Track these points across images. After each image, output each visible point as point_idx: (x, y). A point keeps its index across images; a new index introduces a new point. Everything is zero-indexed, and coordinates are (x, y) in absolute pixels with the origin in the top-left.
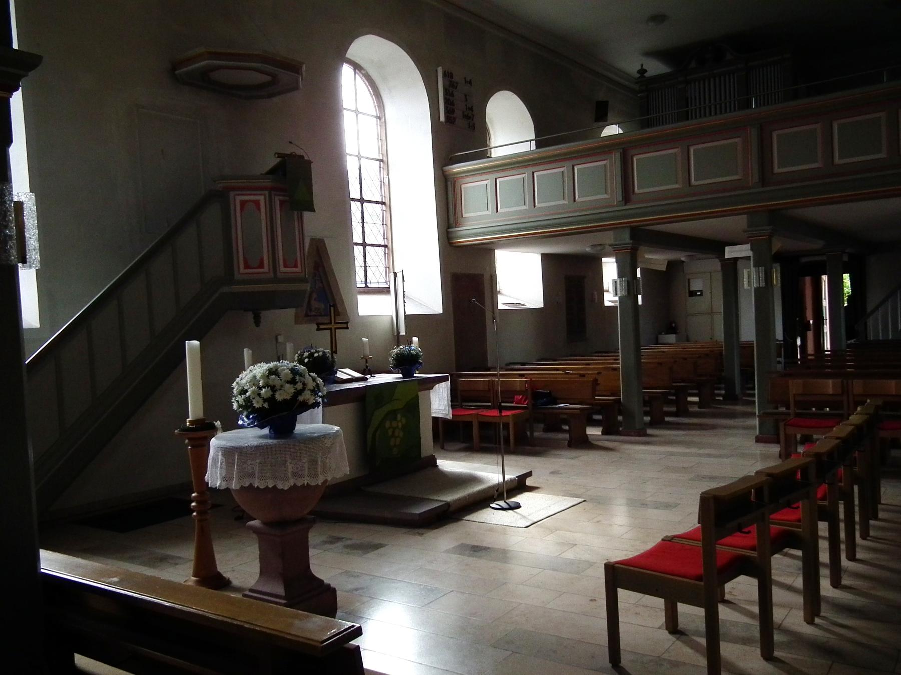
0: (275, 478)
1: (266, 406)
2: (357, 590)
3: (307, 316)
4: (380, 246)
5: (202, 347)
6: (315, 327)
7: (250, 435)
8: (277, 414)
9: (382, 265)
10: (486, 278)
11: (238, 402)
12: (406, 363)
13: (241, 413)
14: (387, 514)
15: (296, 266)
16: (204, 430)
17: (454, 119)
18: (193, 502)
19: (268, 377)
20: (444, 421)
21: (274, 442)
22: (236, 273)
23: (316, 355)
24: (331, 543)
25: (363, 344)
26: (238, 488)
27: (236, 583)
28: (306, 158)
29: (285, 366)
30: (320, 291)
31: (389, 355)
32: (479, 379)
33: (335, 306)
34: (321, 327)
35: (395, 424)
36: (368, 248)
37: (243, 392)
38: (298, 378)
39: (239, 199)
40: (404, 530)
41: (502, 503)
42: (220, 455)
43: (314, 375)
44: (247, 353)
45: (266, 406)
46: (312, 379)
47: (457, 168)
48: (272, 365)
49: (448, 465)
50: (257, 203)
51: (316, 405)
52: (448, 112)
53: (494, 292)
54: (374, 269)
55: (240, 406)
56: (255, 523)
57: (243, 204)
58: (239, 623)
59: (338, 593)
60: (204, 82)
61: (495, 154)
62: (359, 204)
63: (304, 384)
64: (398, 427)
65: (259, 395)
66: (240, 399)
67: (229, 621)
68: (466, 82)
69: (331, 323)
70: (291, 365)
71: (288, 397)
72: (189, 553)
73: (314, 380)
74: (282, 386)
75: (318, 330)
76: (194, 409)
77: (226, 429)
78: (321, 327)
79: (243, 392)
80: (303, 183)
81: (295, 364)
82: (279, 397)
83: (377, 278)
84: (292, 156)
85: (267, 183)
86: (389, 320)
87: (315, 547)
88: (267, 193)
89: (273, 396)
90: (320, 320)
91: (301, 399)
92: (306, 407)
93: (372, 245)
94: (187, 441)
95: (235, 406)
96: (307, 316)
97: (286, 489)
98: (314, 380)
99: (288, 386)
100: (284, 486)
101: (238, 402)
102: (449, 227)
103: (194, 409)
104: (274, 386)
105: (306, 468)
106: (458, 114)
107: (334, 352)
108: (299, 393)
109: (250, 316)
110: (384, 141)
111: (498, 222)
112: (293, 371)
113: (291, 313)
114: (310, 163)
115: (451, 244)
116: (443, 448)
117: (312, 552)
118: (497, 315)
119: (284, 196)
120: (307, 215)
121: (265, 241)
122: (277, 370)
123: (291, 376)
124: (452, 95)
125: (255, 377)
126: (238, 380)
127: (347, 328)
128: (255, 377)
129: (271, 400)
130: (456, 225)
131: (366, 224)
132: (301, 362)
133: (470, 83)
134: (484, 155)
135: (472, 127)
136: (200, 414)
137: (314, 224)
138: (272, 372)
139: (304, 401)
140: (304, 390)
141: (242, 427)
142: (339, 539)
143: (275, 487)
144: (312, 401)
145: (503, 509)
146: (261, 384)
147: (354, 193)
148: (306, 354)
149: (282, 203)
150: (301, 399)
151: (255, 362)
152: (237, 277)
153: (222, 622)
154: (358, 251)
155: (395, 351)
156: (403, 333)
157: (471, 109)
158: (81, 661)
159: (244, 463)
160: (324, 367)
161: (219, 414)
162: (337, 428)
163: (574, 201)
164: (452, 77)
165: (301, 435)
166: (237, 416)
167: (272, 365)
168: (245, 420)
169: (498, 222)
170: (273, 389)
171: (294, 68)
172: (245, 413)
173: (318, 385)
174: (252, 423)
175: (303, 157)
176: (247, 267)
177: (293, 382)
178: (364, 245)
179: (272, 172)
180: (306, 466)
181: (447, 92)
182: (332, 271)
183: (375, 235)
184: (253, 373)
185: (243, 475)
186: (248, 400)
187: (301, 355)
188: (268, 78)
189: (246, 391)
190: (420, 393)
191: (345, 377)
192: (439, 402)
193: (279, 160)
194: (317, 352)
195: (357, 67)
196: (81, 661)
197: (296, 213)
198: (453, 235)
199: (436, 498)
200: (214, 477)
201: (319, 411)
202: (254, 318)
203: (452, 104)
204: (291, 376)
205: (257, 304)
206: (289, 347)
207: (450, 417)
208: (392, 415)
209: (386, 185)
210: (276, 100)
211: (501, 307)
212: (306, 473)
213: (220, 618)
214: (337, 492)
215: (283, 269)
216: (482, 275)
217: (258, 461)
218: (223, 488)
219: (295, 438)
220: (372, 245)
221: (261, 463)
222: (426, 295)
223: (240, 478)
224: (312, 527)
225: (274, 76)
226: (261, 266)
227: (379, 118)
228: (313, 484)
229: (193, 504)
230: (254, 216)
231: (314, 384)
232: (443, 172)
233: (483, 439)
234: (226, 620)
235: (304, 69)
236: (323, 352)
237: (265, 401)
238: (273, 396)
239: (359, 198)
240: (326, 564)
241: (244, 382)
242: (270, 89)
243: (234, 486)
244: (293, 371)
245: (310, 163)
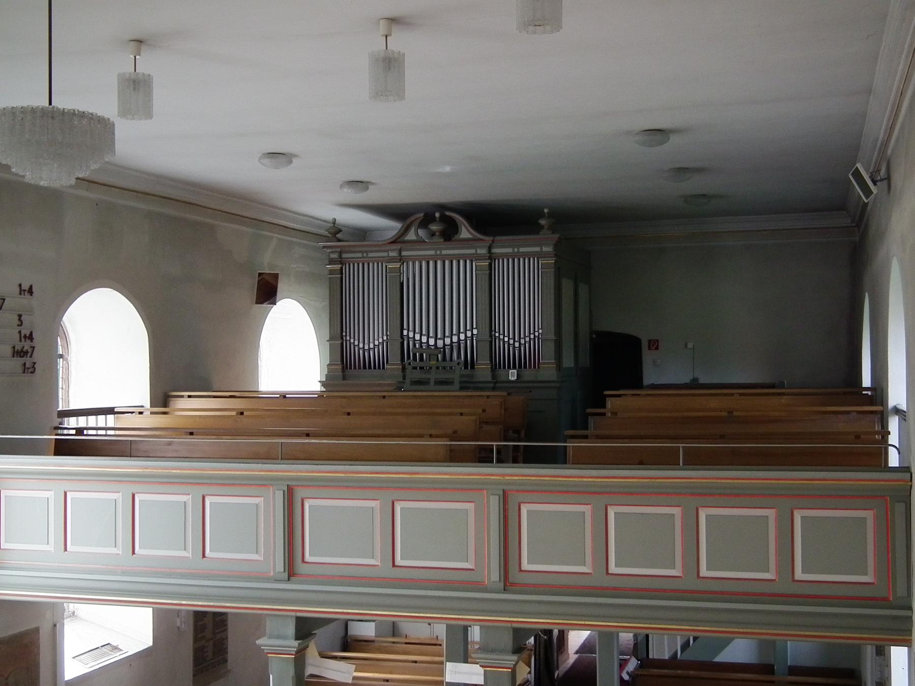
68: (21, 291)
157: (30, 337)
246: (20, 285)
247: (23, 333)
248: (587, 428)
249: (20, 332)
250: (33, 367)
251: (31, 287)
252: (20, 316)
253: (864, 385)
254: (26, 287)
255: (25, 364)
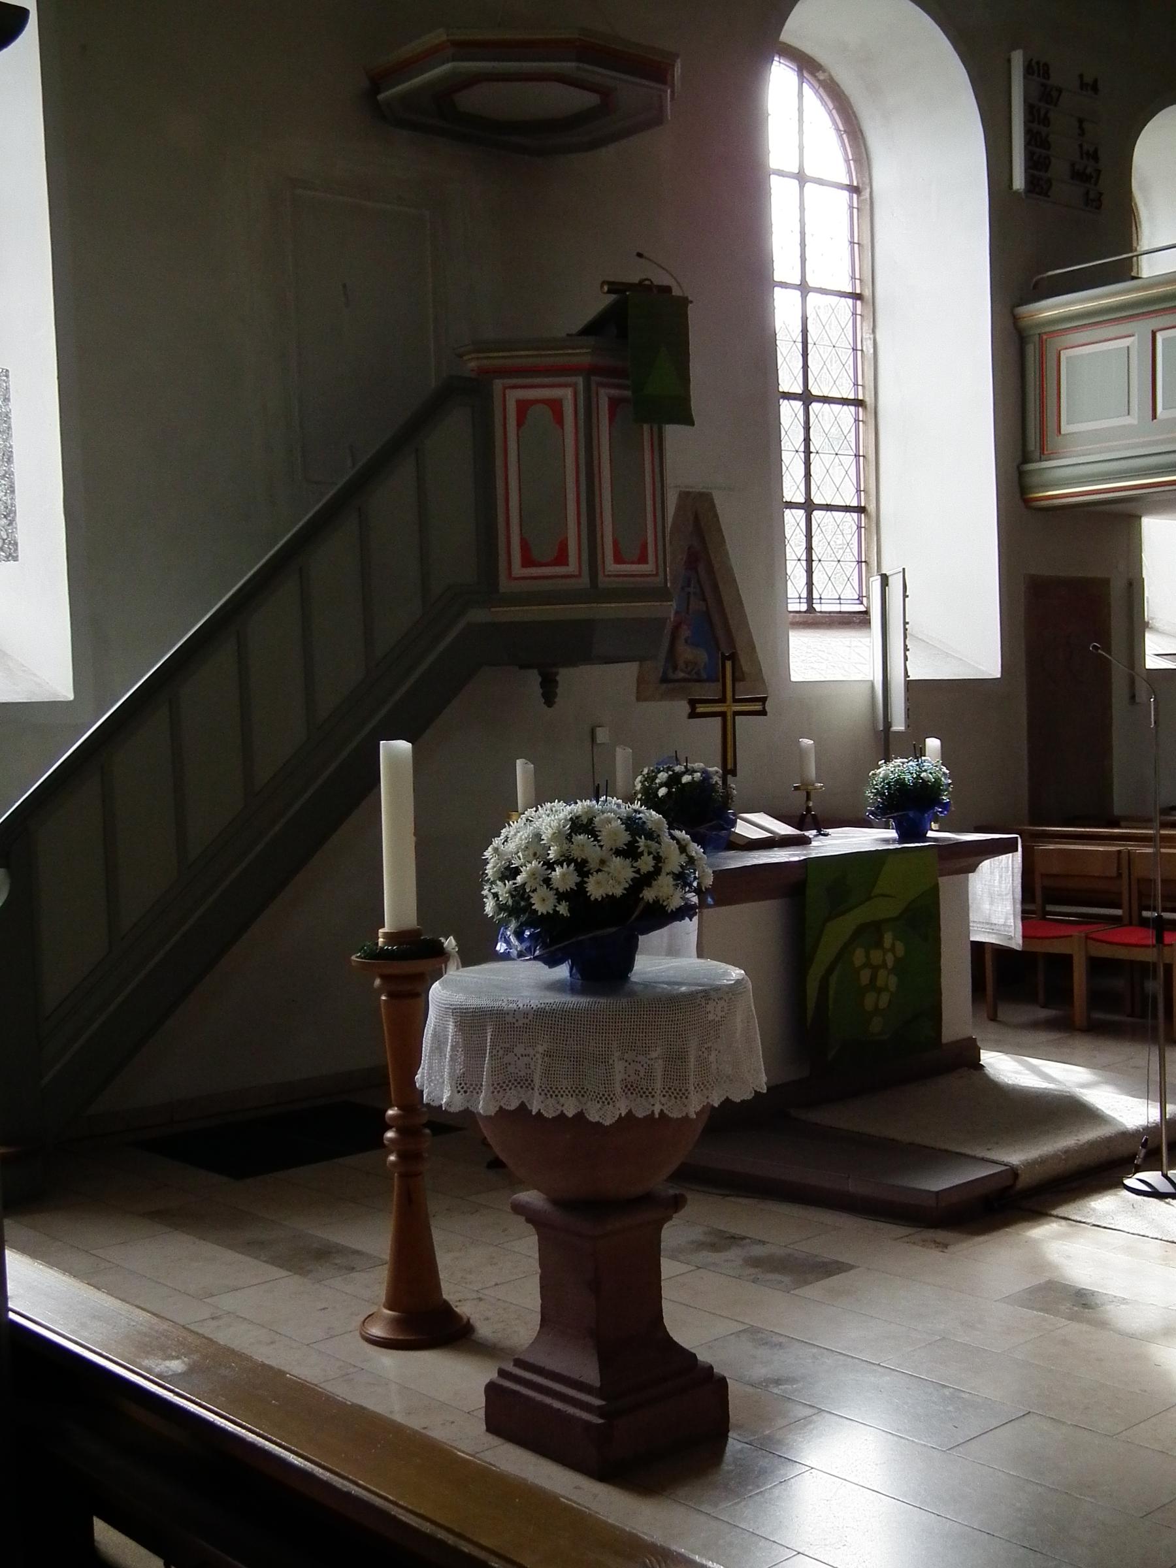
0: (580, 1092)
1: (563, 909)
2: (778, 1382)
3: (665, 680)
4: (847, 509)
5: (418, 755)
6: (683, 707)
7: (521, 980)
8: (592, 932)
9: (851, 556)
10: (1117, 588)
11: (496, 895)
12: (908, 805)
13: (505, 923)
14: (853, 1186)
15: (643, 559)
16: (417, 957)
17: (1049, 182)
18: (388, 1127)
19: (569, 838)
20: (1001, 952)
21: (582, 1001)
22: (503, 578)
23: (686, 779)
24: (713, 1247)
25: (802, 753)
26: (492, 1111)
27: (484, 1330)
28: (676, 292)
29: (612, 809)
30: (706, 633)
31: (866, 780)
32: (1092, 847)
33: (733, 657)
34: (701, 709)
35: (876, 956)
36: (817, 514)
37: (510, 873)
38: (642, 842)
39: (513, 396)
40: (901, 1231)
41: (1153, 1177)
42: (451, 1028)
43: (682, 835)
44: (522, 769)
45: (563, 909)
46: (675, 844)
47: (1051, 309)
48: (579, 807)
49: (1005, 1066)
50: (556, 406)
51: (686, 911)
52: (1034, 163)
53: (1135, 625)
54: (830, 567)
55: (501, 907)
56: (531, 1197)
57: (523, 407)
58: (476, 1552)
59: (732, 1386)
60: (441, 118)
61: (1151, 267)
62: (798, 405)
63: (658, 859)
64: (884, 965)
65: (547, 881)
66: (503, 890)
67: (451, 1540)
68: (1083, 85)
69: (723, 700)
70: (626, 809)
71: (618, 891)
72: (376, 1240)
73: (683, 849)
74: (603, 862)
75: (693, 715)
76: (398, 907)
77: (469, 958)
78: (701, 709)
79: (510, 873)
80: (668, 351)
81: (637, 805)
82: (596, 889)
83: (837, 589)
84: (644, 287)
85: (583, 356)
86: (865, 690)
87: (673, 1258)
88: (580, 380)
89: (581, 886)
90: (699, 691)
91: (649, 895)
92: (660, 916)
93: (829, 508)
94: (378, 982)
95: (489, 907)
96: (665, 680)
97: (607, 1123)
98: (683, 849)
99: (617, 861)
100: (604, 1114)
101: (496, 895)
102: (1026, 458)
103: (398, 907)
104: (585, 862)
105: (659, 1074)
106: (1059, 168)
107: (729, 771)
108: (644, 880)
109: (533, 678)
110: (864, 245)
111: (1143, 445)
112: (633, 825)
113: (630, 670)
114: (684, 302)
115: (1027, 502)
116: (993, 1018)
117: (669, 1268)
118: (1142, 689)
119: (618, 386)
120: (673, 432)
121: (571, 496)
122: (591, 821)
123: (625, 837)
124: (1046, 121)
125: (538, 836)
126: (497, 842)
127: (763, 713)
128: (538, 836)
129: (576, 896)
130: (1043, 454)
131: (815, 456)
132: (650, 799)
133: (1095, 87)
134: (1124, 272)
135: (1094, 202)
136: (410, 920)
137: (689, 456)
138: (580, 826)
139: (656, 901)
140: (657, 871)
141: (506, 957)
142: (734, 1240)
143: (580, 1116)
144: (676, 903)
145: (1155, 1194)
146: (552, 855)
147: (789, 380)
148: (663, 776)
149: (614, 403)
150: (649, 895)
151: (539, 799)
152: (505, 585)
153: (430, 1539)
154: (793, 520)
155: (882, 772)
156: (899, 725)
157: (1094, 156)
158: (105, 1535)
159: (508, 1051)
160: (701, 810)
161: (453, 925)
162: (736, 973)
163: (1154, 417)
164: (1047, 75)
165: (647, 985)
166: (491, 931)
167: (579, 807)
168: (513, 939)
169: (1156, 443)
170: (582, 868)
171: (653, 69)
172: (513, 925)
173: (691, 861)
174: (529, 950)
175: (668, 289)
176: (528, 561)
177: (630, 852)
178: (809, 506)
179: (592, 329)
180: (659, 1066)
181: (1033, 114)
182: (729, 570)
183: (835, 481)
184: (534, 826)
185: (505, 1081)
186: (520, 894)
187: (651, 778)
188: (590, 99)
189: (517, 872)
190: (940, 879)
191: (755, 834)
192: (993, 900)
193: (613, 297)
194: (687, 771)
195: (807, 65)
196: (105, 1535)
197: (646, 427)
198: (1034, 480)
199: (980, 1153)
200: (437, 1080)
201: (690, 926)
202: (542, 685)
203: (1045, 144)
204: (625, 837)
205: (550, 651)
206: (623, 756)
207: (1017, 943)
208: (870, 933)
209: (866, 359)
210: (607, 154)
211: (1152, 663)
212: (659, 1085)
213: (427, 1528)
214: (727, 1120)
215: (612, 567)
216: (1106, 582)
217: (540, 1049)
218: (456, 1108)
219: (632, 994)
220: (829, 508)
221: (548, 1054)
222: (961, 628)
223: (499, 1087)
224: (669, 1218)
225: (606, 94)
226: (561, 558)
227: (855, 190)
228: (675, 1115)
229: (390, 1134)
230: (549, 432)
231: (683, 859)
232: (1015, 319)
233: (1097, 998)
234: (442, 1535)
235: (678, 70)
236: (704, 772)
237: (561, 896)
238: (581, 886)
239: (798, 389)
240: (703, 1306)
241: (511, 846)
242: (590, 129)
243: (483, 1105)
244: (633, 825)
245: (684, 302)
246: (1081, 76)
247: (1085, 147)
248: (1067, 960)
249: (1081, 146)
250: (1099, 200)
251: (1096, 81)
252: (1081, 121)
253: (784, 387)
254: (1088, 79)
255: (1087, 193)
